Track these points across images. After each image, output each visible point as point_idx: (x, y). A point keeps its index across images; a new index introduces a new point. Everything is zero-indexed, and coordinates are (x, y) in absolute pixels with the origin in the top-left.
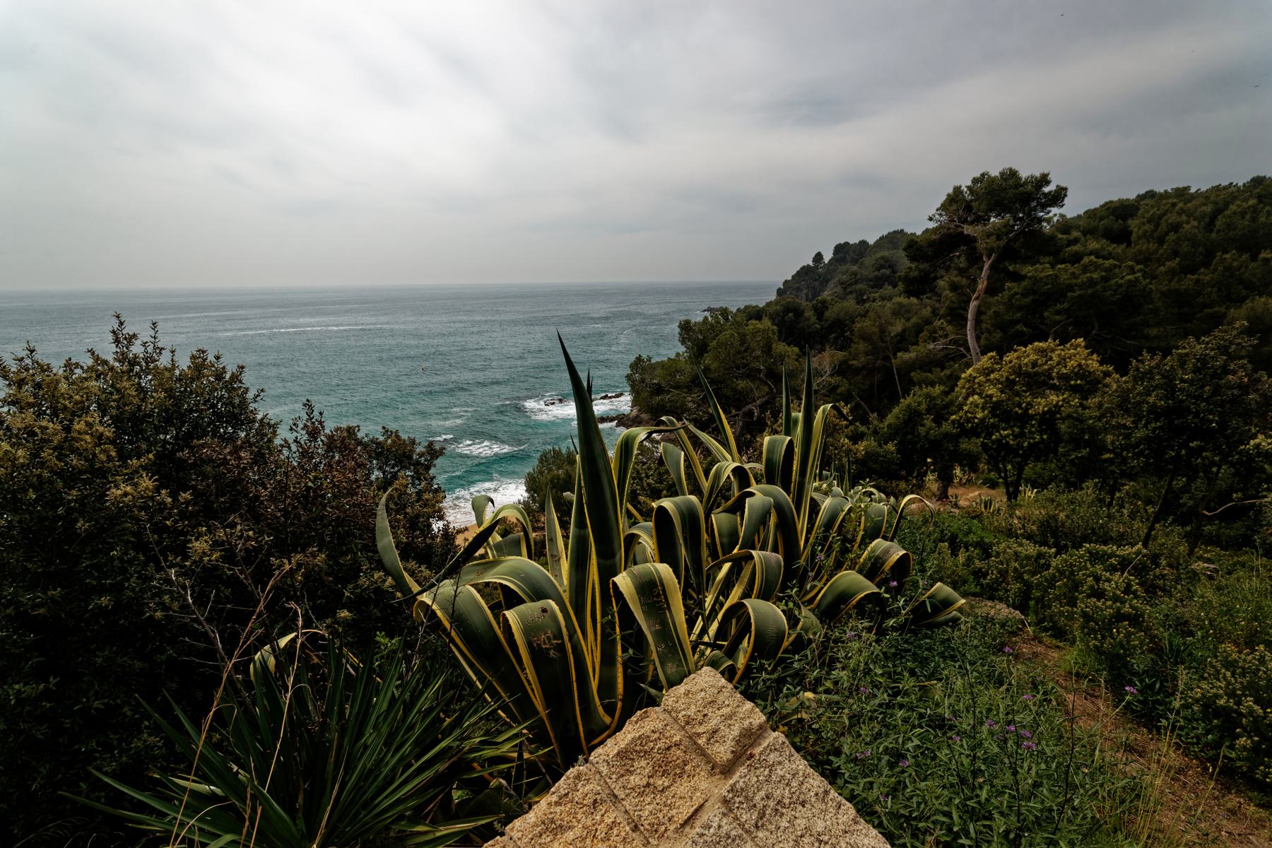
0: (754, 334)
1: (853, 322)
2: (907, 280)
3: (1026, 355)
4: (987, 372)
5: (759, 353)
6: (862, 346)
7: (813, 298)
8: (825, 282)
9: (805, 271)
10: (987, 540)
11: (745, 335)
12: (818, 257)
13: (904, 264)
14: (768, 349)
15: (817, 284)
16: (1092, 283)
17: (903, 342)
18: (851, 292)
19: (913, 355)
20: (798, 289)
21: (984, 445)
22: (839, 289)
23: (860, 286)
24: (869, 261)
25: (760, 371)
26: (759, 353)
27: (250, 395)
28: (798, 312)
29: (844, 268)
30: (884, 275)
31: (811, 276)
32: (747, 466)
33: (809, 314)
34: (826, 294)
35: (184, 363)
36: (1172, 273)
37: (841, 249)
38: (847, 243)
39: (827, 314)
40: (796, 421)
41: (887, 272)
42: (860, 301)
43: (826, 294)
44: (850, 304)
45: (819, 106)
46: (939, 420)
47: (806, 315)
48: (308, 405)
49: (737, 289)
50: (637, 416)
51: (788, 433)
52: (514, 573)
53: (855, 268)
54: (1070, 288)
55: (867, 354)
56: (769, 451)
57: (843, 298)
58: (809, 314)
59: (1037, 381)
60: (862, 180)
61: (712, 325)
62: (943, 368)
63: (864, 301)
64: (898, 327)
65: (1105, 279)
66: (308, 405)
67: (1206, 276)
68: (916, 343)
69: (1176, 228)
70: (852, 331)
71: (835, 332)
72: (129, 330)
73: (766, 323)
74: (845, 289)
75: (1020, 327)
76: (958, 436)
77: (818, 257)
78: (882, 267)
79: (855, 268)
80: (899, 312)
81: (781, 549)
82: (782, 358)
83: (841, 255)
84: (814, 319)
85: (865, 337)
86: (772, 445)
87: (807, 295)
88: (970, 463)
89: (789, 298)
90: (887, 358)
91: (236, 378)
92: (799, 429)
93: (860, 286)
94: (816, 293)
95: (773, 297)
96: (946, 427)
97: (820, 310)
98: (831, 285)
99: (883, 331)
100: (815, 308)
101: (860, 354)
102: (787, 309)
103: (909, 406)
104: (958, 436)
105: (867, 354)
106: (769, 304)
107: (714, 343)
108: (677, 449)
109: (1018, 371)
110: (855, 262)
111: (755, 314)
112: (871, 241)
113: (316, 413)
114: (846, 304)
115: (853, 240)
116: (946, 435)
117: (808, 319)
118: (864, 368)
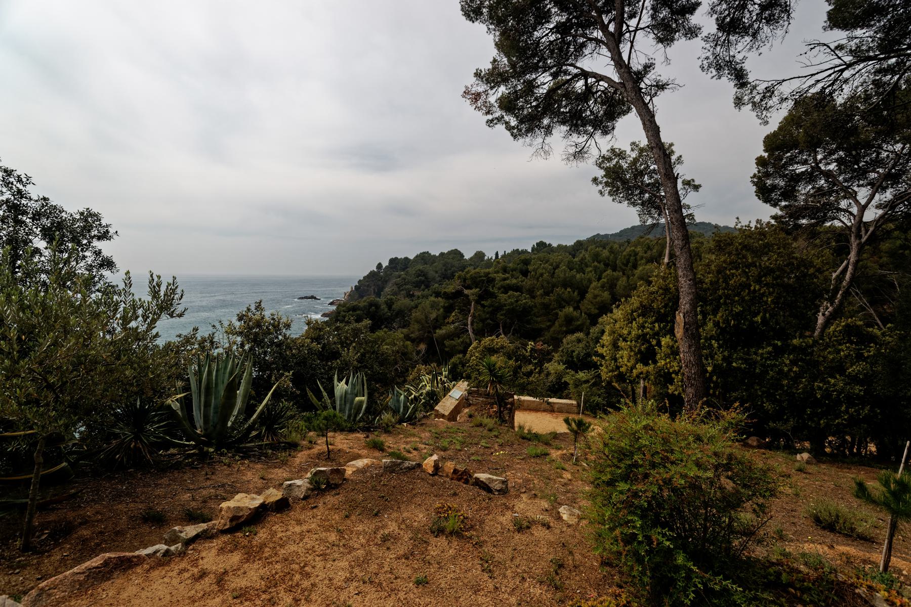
3: (486, 341)
4: (475, 348)
6: (416, 326)
8: (385, 281)
9: (372, 274)
10: (665, 418)
16: (512, 304)
19: (444, 331)
22: (395, 288)
23: (407, 287)
24: (412, 271)
30: (423, 281)
31: (375, 280)
33: (383, 306)
36: (542, 295)
37: (393, 261)
38: (396, 258)
39: (394, 307)
41: (423, 278)
45: (377, 158)
54: (505, 305)
55: (419, 330)
58: (383, 306)
59: (491, 351)
60: (400, 209)
62: (459, 338)
64: (433, 316)
65: (517, 301)
67: (552, 297)
69: (542, 275)
75: (489, 321)
78: (419, 275)
81: (234, 523)
84: (386, 310)
85: (418, 322)
93: (407, 287)
97: (390, 304)
99: (426, 317)
105: (419, 330)
109: (485, 347)
110: (403, 270)
112: (412, 257)
115: (401, 256)
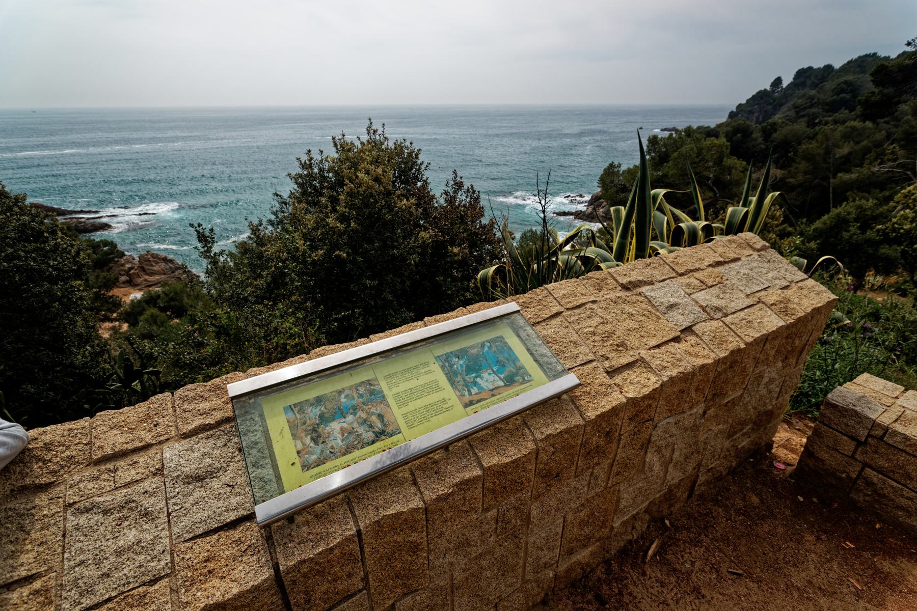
0: (710, 149)
1: (800, 144)
2: (867, 104)
5: (711, 164)
6: (803, 166)
7: (764, 121)
9: (761, 96)
11: (702, 149)
12: (778, 81)
13: (868, 86)
14: (719, 161)
15: (770, 107)
17: (846, 164)
18: (803, 116)
19: (854, 176)
20: (751, 112)
21: (904, 253)
22: (792, 113)
24: (829, 85)
25: (709, 178)
26: (711, 164)
27: (423, 167)
28: (745, 132)
29: (801, 92)
32: (713, 225)
33: (757, 135)
34: (777, 118)
35: (391, 145)
39: (775, 135)
40: (751, 202)
42: (811, 124)
43: (777, 118)
44: (801, 126)
46: (863, 228)
47: (754, 136)
48: (455, 172)
49: (351, 117)
50: (592, 213)
51: (744, 205)
52: (593, 252)
53: (813, 92)
56: (730, 216)
57: (793, 121)
58: (757, 135)
61: (675, 141)
63: (815, 125)
66: (455, 172)
68: (861, 166)
70: (796, 152)
71: (784, 151)
72: (374, 127)
73: (723, 140)
74: (797, 113)
76: (881, 243)
77: (778, 81)
78: (843, 91)
79: (813, 92)
80: (851, 135)
82: (730, 169)
83: (802, 79)
84: (760, 140)
86: (733, 214)
87: (758, 118)
88: (886, 268)
89: (741, 120)
90: (826, 179)
91: (417, 155)
92: (753, 206)
94: (768, 116)
95: (724, 120)
96: (869, 234)
98: (784, 108)
100: (764, 130)
101: (800, 172)
102: (736, 130)
103: (838, 215)
104: (881, 243)
105: (806, 173)
106: (719, 126)
107: (676, 154)
108: (662, 215)
111: (710, 133)
113: (458, 179)
114: (796, 127)
116: (869, 242)
117: (756, 139)
118: (800, 185)
